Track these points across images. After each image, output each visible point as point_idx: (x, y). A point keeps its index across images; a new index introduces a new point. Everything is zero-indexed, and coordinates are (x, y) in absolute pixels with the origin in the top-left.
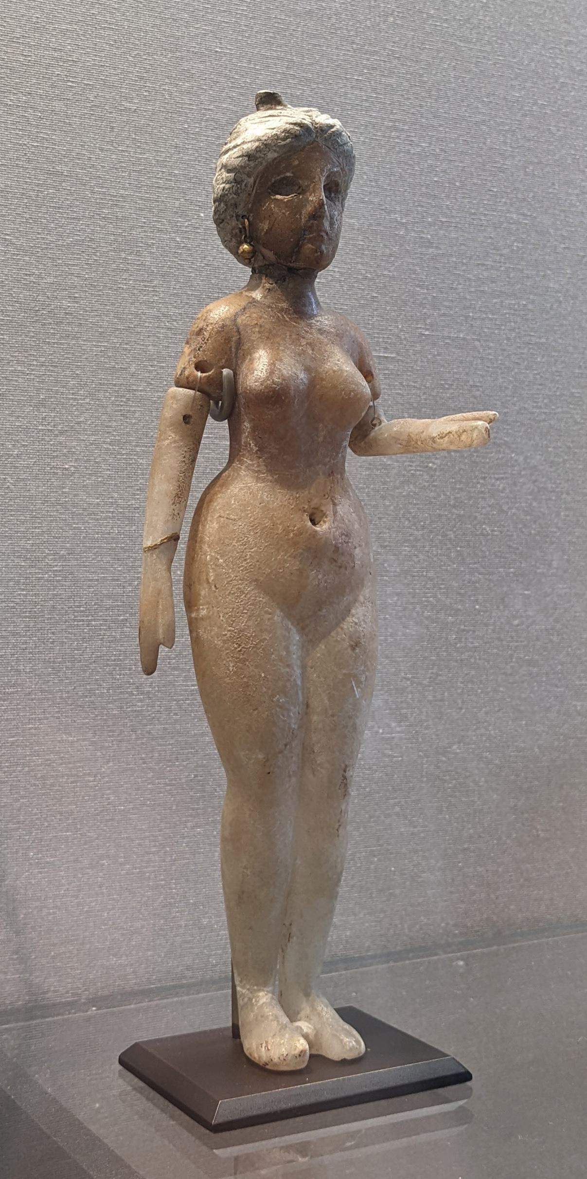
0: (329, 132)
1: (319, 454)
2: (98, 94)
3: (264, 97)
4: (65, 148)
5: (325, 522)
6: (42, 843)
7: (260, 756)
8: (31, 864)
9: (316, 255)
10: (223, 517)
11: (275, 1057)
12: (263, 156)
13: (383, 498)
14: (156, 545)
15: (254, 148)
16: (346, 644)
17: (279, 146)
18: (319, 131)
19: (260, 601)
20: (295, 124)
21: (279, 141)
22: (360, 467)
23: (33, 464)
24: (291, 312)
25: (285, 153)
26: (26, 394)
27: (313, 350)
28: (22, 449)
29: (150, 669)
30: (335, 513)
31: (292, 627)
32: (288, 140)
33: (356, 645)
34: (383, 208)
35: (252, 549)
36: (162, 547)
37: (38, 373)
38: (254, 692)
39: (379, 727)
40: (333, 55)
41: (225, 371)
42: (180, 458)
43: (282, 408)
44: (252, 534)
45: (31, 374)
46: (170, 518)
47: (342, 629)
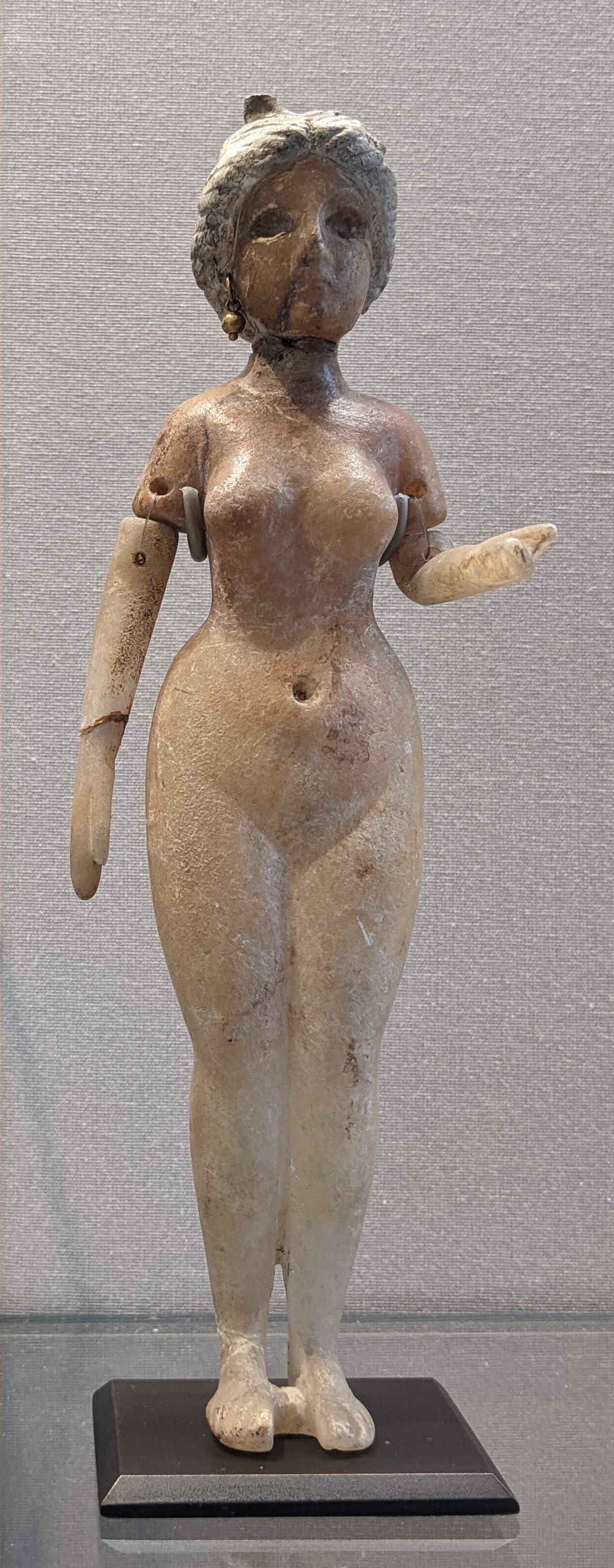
0: (334, 138)
1: (314, 600)
2: (174, 153)
3: (251, 103)
4: (129, 229)
5: (317, 695)
6: (99, 1112)
7: (218, 1016)
8: (83, 1136)
9: (311, 316)
10: (179, 690)
11: (227, 1430)
12: (237, 184)
13: (599, 675)
14: (89, 727)
15: (224, 175)
16: (349, 868)
17: (256, 168)
18: (317, 139)
19: (218, 804)
20: (279, 133)
21: (256, 160)
22: (562, 632)
23: (85, 637)
24: (288, 402)
25: (266, 176)
26: (76, 548)
27: (309, 452)
28: (71, 618)
29: (87, 890)
30: (336, 684)
31: (267, 842)
32: (268, 156)
33: (366, 871)
34: (601, 262)
35: (209, 732)
36: (97, 730)
37: (93, 521)
38: (206, 928)
39: (589, 1000)
40: (521, 54)
41: (186, 490)
42: (125, 611)
43: (249, 537)
44: (211, 711)
45: (83, 522)
46: (108, 692)
47: (344, 846)
